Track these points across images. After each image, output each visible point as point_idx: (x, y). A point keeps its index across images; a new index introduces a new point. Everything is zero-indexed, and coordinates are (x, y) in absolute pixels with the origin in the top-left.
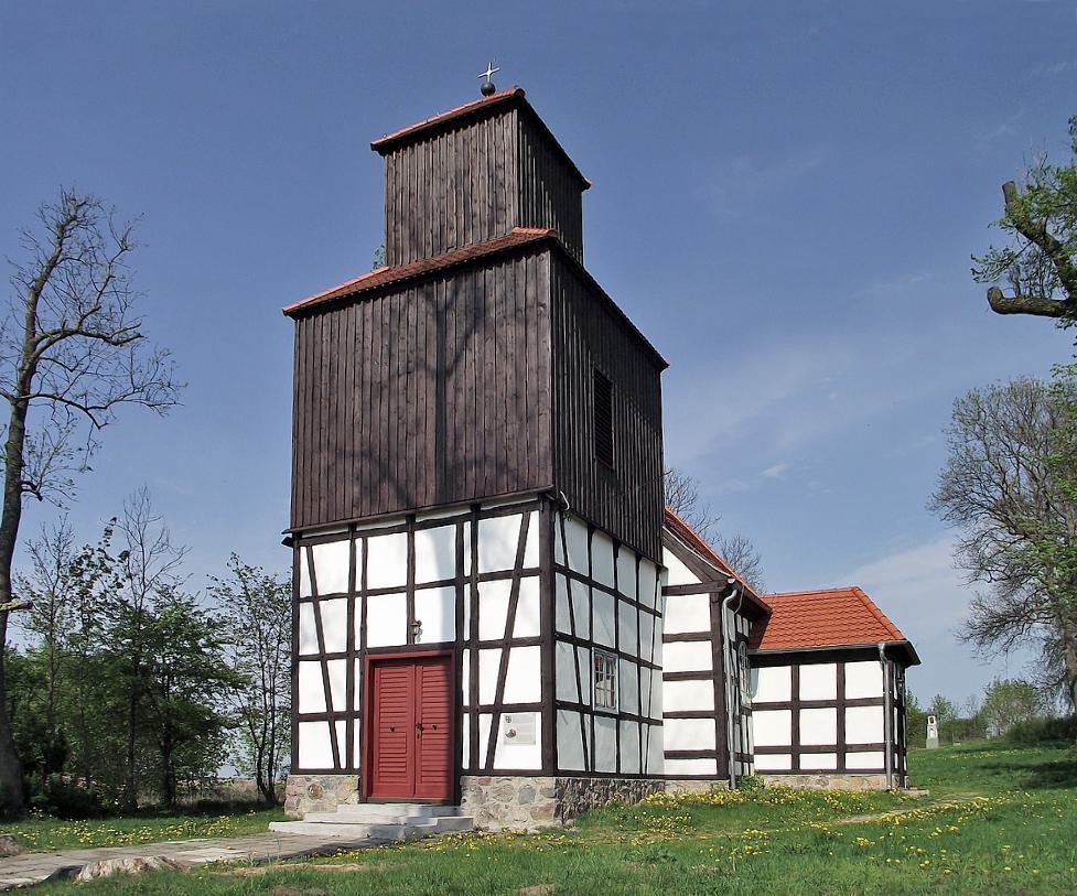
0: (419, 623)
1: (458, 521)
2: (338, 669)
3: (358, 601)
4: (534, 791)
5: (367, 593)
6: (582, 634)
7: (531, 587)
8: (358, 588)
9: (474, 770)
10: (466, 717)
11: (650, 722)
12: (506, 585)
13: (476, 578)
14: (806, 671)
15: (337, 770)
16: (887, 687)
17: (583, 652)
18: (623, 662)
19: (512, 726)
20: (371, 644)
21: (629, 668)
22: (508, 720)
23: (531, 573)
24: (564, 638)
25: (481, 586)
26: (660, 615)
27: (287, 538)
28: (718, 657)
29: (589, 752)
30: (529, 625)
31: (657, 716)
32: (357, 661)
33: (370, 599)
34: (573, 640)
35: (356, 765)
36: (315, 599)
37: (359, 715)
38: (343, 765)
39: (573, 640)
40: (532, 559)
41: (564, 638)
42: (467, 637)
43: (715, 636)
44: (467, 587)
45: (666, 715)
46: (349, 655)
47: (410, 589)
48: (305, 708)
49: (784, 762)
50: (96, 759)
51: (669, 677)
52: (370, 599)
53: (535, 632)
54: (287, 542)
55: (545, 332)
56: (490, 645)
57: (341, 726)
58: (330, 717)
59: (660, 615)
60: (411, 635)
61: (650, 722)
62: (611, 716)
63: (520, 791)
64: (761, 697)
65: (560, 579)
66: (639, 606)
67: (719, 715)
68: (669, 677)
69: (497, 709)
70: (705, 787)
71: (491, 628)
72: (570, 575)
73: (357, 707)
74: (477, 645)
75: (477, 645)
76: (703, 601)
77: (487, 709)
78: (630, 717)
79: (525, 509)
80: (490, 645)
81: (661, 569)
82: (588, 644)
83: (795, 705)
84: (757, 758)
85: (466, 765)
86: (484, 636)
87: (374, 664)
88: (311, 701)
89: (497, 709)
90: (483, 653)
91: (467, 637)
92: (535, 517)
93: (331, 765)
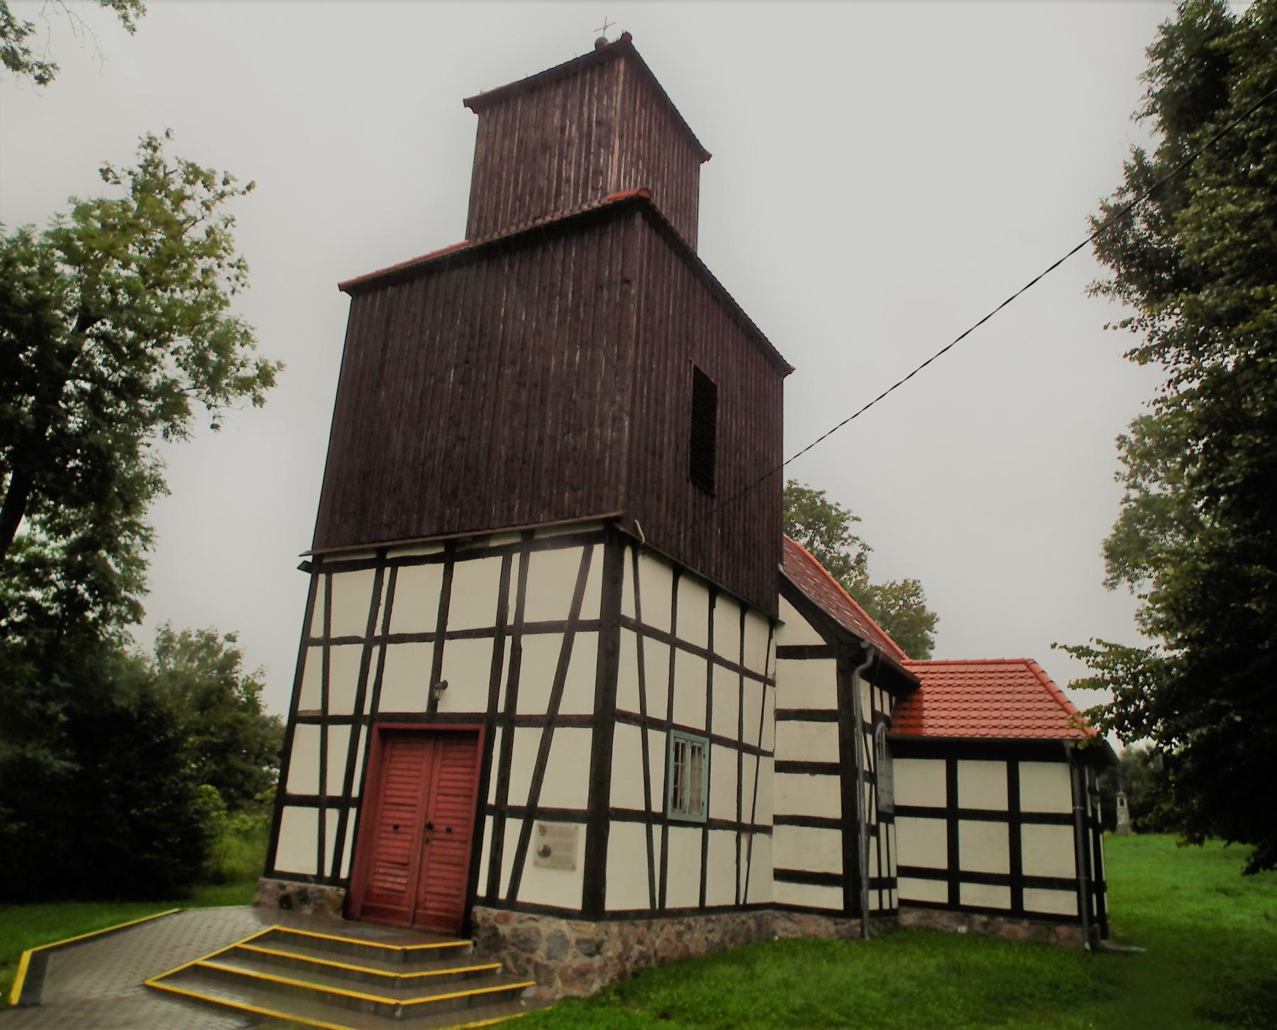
0: (445, 685)
1: (506, 552)
2: (340, 735)
4: (567, 942)
5: (522, 628)
6: (657, 710)
7: (587, 645)
8: (378, 632)
9: (491, 899)
10: (489, 821)
11: (754, 829)
12: (558, 639)
13: (522, 628)
14: (966, 769)
15: (319, 878)
16: (1078, 800)
17: (657, 739)
18: (716, 748)
19: (548, 841)
20: (383, 708)
21: (723, 759)
22: (543, 831)
23: (588, 626)
24: (627, 718)
25: (526, 640)
26: (772, 683)
27: (305, 562)
28: (847, 745)
29: (658, 882)
30: (580, 699)
31: (764, 819)
32: (364, 729)
33: (390, 648)
34: (644, 722)
35: (344, 874)
37: (358, 803)
38: (328, 872)
39: (644, 722)
40: (591, 609)
41: (627, 718)
42: (501, 708)
43: (844, 715)
44: (508, 640)
45: (779, 820)
47: (440, 636)
48: (293, 788)
49: (937, 892)
51: (782, 767)
52: (390, 647)
53: (588, 709)
54: (305, 567)
56: (530, 721)
57: (332, 815)
58: (320, 802)
59: (773, 683)
60: (433, 702)
61: (754, 829)
62: (695, 825)
63: (549, 939)
64: (903, 797)
65: (627, 638)
66: (743, 672)
67: (848, 824)
68: (782, 767)
69: (531, 813)
70: (825, 926)
71: (533, 700)
72: (642, 630)
73: (355, 792)
74: (511, 720)
75: (511, 720)
76: (828, 667)
77: (516, 812)
78: (724, 825)
79: (588, 541)
80: (530, 721)
81: (774, 623)
82: (665, 725)
83: (952, 814)
84: (902, 882)
85: (482, 891)
86: (522, 709)
88: (302, 780)
89: (531, 813)
90: (518, 731)
91: (501, 708)
92: (599, 551)
93: (314, 871)
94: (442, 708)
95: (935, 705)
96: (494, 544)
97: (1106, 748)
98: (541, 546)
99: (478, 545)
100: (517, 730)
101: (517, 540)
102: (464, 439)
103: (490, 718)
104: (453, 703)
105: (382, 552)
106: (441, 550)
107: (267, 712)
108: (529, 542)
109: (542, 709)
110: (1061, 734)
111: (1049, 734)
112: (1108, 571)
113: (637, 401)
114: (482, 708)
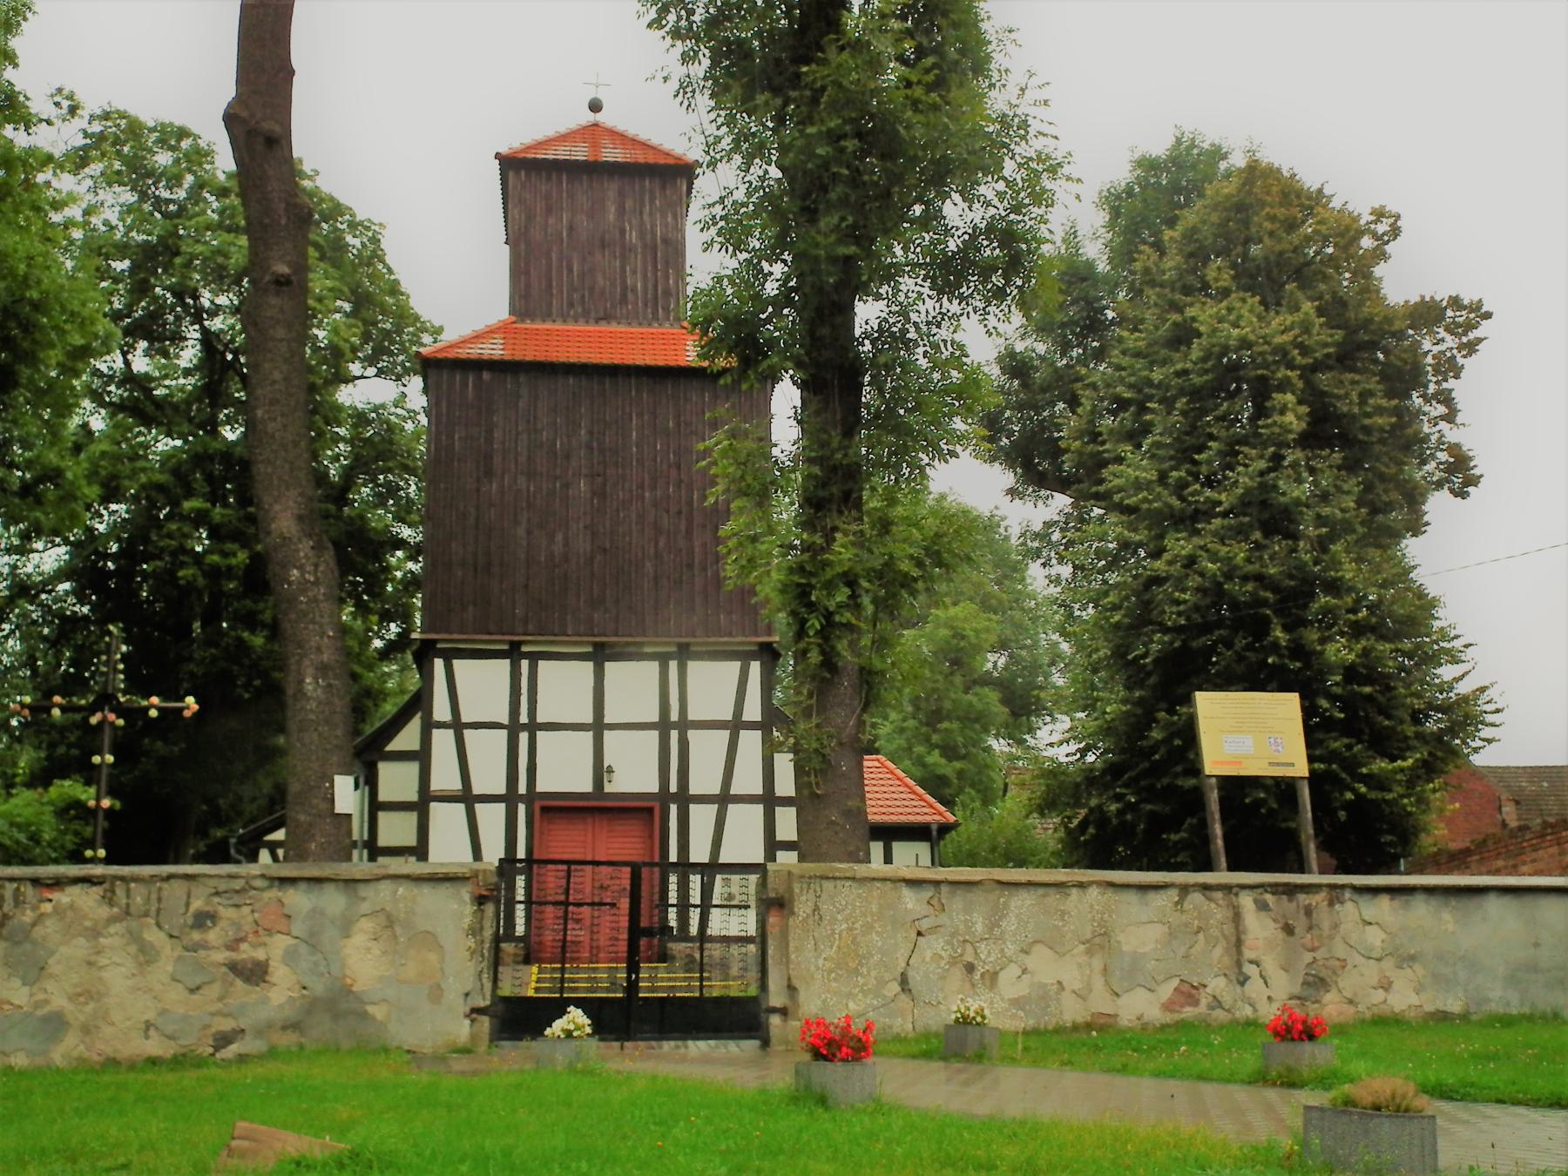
2: (492, 818)
3: (524, 737)
8: (524, 719)
20: (542, 786)
25: (692, 734)
36: (458, 726)
42: (673, 788)
46: (509, 798)
50: (695, 325)
55: (839, 870)
56: (703, 799)
71: (704, 779)
74: (685, 799)
79: (745, 657)
80: (703, 799)
86: (694, 789)
87: (545, 810)
91: (673, 788)
92: (755, 667)
94: (608, 788)
95: (874, 782)
96: (648, 650)
97: (1193, 816)
98: (700, 656)
99: (632, 649)
100: (778, 809)
101: (673, 649)
102: (605, 550)
103: (664, 796)
104: (622, 783)
105: (515, 646)
106: (590, 649)
107: (350, 780)
108: (684, 653)
109: (715, 788)
110: (928, 819)
111: (920, 819)
112: (943, 497)
113: (1220, 842)
114: (654, 787)
